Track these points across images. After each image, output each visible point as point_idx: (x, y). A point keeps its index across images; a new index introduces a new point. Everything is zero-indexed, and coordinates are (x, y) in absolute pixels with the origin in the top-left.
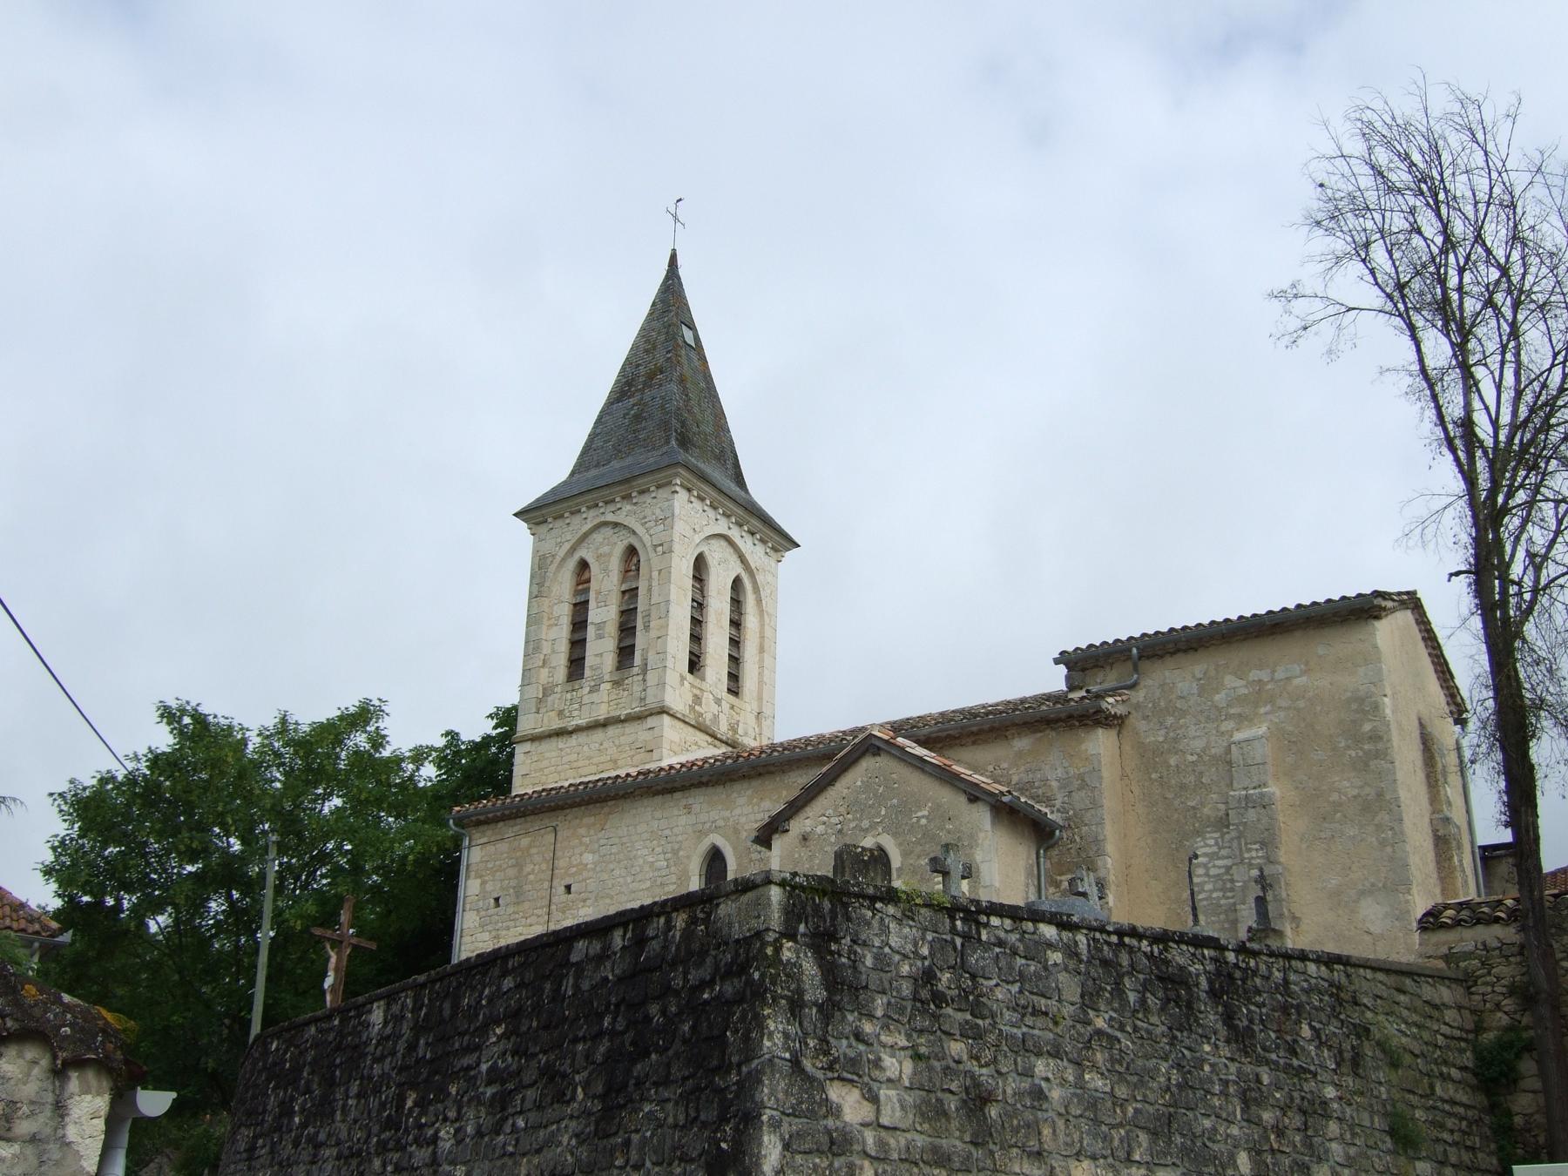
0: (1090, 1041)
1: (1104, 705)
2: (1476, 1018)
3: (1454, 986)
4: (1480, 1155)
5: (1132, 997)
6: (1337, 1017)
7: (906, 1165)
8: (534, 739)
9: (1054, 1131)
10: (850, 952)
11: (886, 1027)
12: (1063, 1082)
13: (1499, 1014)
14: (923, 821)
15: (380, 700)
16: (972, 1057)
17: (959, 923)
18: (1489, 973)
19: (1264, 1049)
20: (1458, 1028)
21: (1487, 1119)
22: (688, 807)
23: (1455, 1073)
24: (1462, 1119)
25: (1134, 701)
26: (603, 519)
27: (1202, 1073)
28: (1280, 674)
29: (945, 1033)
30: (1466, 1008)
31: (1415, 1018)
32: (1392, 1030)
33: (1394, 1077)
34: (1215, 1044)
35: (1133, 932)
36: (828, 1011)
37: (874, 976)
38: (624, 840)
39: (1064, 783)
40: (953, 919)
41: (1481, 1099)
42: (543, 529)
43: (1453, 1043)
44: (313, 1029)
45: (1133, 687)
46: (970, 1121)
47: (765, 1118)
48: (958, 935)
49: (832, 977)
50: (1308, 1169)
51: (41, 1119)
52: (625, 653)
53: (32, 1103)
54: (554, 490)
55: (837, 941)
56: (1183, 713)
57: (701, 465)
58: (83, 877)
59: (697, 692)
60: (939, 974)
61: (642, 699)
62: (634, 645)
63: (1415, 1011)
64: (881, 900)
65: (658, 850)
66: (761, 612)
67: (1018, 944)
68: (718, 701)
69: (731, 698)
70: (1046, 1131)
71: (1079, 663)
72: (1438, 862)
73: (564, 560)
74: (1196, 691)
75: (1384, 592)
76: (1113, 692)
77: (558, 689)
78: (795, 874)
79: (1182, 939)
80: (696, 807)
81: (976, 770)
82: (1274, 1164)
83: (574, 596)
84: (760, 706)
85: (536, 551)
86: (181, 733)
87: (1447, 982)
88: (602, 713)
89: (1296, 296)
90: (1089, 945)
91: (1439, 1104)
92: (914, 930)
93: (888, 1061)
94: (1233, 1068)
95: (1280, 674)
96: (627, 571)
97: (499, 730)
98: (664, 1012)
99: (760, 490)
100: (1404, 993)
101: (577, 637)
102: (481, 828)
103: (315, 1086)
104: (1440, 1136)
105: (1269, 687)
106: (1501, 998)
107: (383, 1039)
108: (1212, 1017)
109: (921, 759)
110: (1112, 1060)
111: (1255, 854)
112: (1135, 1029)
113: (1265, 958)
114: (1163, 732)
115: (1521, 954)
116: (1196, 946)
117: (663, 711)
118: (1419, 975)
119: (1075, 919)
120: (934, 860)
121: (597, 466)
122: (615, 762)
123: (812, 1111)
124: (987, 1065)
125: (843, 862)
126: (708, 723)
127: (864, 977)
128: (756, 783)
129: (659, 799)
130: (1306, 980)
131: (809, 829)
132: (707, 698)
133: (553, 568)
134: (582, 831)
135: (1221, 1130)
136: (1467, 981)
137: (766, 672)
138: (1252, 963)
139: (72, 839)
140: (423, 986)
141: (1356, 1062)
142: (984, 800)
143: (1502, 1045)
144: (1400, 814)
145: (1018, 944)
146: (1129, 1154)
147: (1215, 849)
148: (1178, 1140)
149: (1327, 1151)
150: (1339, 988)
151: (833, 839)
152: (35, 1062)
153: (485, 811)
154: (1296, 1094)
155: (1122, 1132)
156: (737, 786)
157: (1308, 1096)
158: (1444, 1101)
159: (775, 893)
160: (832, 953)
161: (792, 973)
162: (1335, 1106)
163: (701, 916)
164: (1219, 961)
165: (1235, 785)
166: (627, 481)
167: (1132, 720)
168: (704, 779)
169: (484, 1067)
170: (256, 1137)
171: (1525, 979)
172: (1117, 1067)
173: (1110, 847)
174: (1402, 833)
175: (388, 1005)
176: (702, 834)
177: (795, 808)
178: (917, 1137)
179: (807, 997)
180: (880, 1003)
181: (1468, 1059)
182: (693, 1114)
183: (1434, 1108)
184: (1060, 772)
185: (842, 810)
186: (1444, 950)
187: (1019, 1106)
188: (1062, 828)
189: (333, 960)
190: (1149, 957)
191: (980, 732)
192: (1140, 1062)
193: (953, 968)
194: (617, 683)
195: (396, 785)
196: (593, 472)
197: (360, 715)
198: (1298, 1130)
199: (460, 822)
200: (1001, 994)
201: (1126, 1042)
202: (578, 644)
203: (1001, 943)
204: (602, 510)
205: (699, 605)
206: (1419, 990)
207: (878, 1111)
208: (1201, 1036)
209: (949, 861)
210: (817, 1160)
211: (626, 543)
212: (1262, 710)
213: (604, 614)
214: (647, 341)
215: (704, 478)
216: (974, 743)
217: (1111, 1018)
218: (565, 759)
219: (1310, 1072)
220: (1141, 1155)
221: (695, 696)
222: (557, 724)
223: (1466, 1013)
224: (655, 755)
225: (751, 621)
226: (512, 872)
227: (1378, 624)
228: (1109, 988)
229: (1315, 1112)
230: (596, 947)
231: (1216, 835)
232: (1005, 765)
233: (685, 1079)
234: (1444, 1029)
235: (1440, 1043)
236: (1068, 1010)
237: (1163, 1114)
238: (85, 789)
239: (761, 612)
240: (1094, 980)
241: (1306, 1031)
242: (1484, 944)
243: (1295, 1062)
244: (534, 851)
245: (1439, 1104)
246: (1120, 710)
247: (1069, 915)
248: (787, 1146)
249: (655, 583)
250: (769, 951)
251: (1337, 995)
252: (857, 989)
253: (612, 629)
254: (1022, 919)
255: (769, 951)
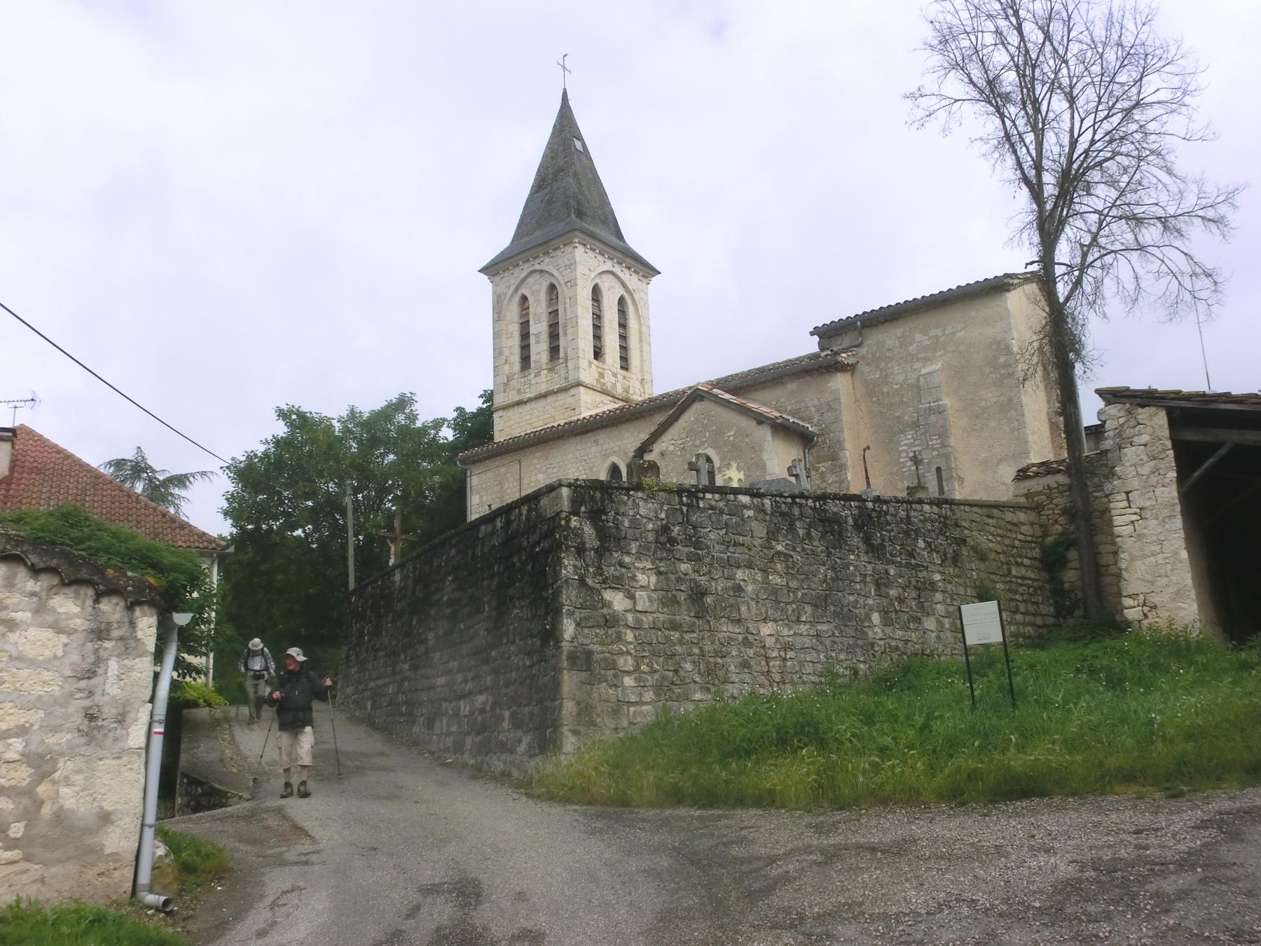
0: (772, 558)
1: (839, 359)
2: (1043, 529)
3: (1029, 512)
4: (1041, 607)
5: (801, 532)
6: (944, 535)
7: (654, 631)
8: (505, 408)
9: (749, 608)
10: (614, 520)
11: (638, 558)
12: (755, 581)
13: (1057, 526)
14: (731, 438)
15: (411, 393)
16: (695, 571)
17: (684, 499)
18: (1051, 503)
19: (891, 555)
20: (1030, 536)
21: (1048, 586)
22: (596, 441)
23: (1026, 561)
24: (1029, 587)
25: (860, 354)
26: (533, 268)
27: (848, 571)
28: (949, 331)
29: (676, 559)
30: (1036, 524)
31: (999, 531)
32: (983, 540)
33: (982, 566)
34: (858, 554)
35: (802, 496)
36: (601, 552)
37: (630, 532)
38: (561, 464)
39: (819, 409)
40: (681, 497)
41: (1044, 575)
42: (497, 278)
43: (1026, 545)
44: (370, 588)
45: (859, 346)
46: (694, 606)
47: (564, 611)
48: (684, 505)
49: (603, 534)
50: (920, 619)
51: (124, 629)
52: (554, 350)
53: (118, 622)
54: (502, 253)
55: (606, 514)
56: (891, 359)
57: (592, 228)
58: (246, 514)
59: (601, 370)
60: (672, 528)
61: (566, 378)
62: (559, 346)
63: (1000, 528)
64: (633, 489)
65: (581, 468)
66: (639, 317)
67: (724, 507)
68: (615, 375)
69: (624, 372)
70: (743, 608)
71: (827, 333)
72: (1052, 439)
73: (512, 296)
74: (897, 345)
75: (1013, 274)
76: (846, 350)
77: (516, 376)
78: (577, 480)
79: (835, 497)
80: (601, 441)
81: (765, 404)
82: (896, 619)
83: (521, 318)
84: (643, 375)
85: (494, 293)
86: (291, 425)
87: (1024, 510)
88: (543, 388)
89: (921, 96)
90: (772, 505)
91: (1014, 579)
92: (655, 505)
93: (640, 576)
94: (870, 567)
95: (949, 331)
96: (551, 300)
97: (486, 405)
98: (520, 560)
99: (635, 238)
100: (993, 518)
101: (525, 343)
102: (476, 465)
103: (373, 619)
104: (1013, 597)
105: (943, 339)
106: (1058, 516)
107: (401, 589)
108: (856, 540)
109: (727, 401)
110: (787, 567)
111: (935, 442)
112: (803, 550)
113: (894, 504)
114: (878, 372)
115: (1069, 490)
116: (845, 501)
117: (579, 384)
118: (1004, 507)
119: (762, 491)
120: (690, 464)
121: (527, 235)
122: (554, 417)
123: (593, 606)
124: (704, 575)
125: (631, 469)
126: (609, 388)
127: (623, 532)
128: (635, 423)
129: (579, 438)
130: (922, 515)
131: (664, 449)
132: (608, 374)
133: (506, 302)
134: (535, 461)
135: (861, 602)
136: (1038, 508)
137: (645, 354)
138: (885, 508)
139: (238, 493)
140: (416, 558)
141: (956, 559)
142: (767, 423)
143: (1057, 544)
144: (1023, 411)
145: (724, 507)
146: (798, 618)
147: (912, 441)
148: (832, 608)
149: (933, 609)
150: (946, 518)
151: (679, 453)
152: (117, 604)
153: (477, 454)
154: (913, 580)
155: (794, 606)
156: (624, 426)
157: (922, 580)
158: (1017, 577)
159: (565, 491)
160: (603, 521)
161: (578, 533)
162: (940, 584)
163: (534, 506)
164: (862, 509)
165: (923, 400)
166: (545, 243)
167: (859, 366)
168: (604, 424)
169: (445, 599)
170: (349, 650)
171: (1072, 504)
172: (791, 571)
173: (848, 445)
174: (1024, 422)
175: (402, 570)
176: (605, 456)
177: (655, 437)
178: (660, 615)
179: (587, 546)
180: (634, 547)
181: (1037, 553)
182: (534, 612)
183: (1011, 582)
184: (816, 402)
185: (683, 435)
186: (1025, 491)
187: (726, 596)
188: (818, 435)
189: (393, 549)
190: (813, 509)
191: (765, 382)
192: (806, 568)
193: (682, 523)
194: (550, 370)
195: (426, 443)
196: (525, 239)
197: (399, 404)
198: (914, 598)
199: (464, 462)
200: (712, 536)
201: (797, 557)
202: (525, 348)
203: (712, 508)
204: (532, 263)
205: (598, 317)
206: (1003, 516)
207: (635, 603)
208: (848, 551)
209: (699, 463)
210: (598, 631)
211: (548, 282)
212: (939, 354)
213: (539, 328)
214: (552, 151)
215: (593, 236)
216: (764, 388)
217: (787, 544)
218: (524, 419)
219: (923, 566)
220: (806, 618)
221: (600, 373)
222: (517, 398)
223: (1037, 527)
224: (577, 412)
225: (632, 323)
226: (496, 489)
227: (1008, 295)
228: (785, 528)
229: (926, 588)
230: (490, 528)
231: (912, 432)
232: (783, 400)
233: (530, 594)
234: (1020, 537)
235: (1016, 545)
236: (757, 542)
237: (822, 595)
238: (241, 462)
239: (639, 317)
240: (775, 524)
241: (921, 544)
242: (1048, 486)
243: (913, 562)
244: (508, 475)
245: (1014, 579)
246: (851, 361)
247: (757, 489)
248: (578, 625)
249: (568, 306)
250: (563, 523)
251: (944, 522)
252: (619, 539)
253: (545, 337)
254: (726, 494)
255: (563, 523)
